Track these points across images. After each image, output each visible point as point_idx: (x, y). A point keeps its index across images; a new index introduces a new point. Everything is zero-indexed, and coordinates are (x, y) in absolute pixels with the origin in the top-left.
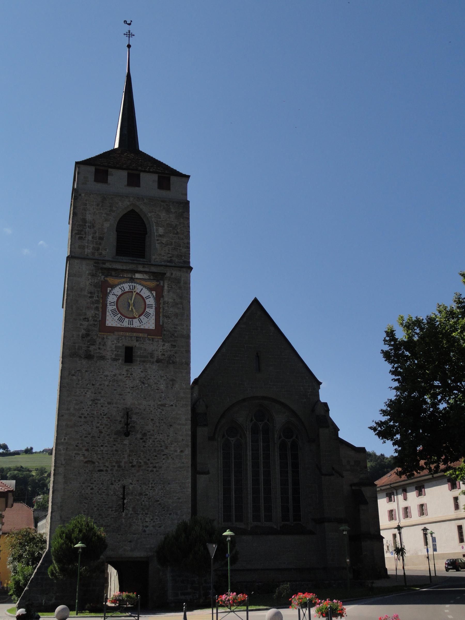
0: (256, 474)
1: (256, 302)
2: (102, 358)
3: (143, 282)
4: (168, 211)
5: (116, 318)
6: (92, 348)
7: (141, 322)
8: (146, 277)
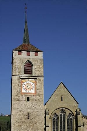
2: (22, 100)
7: (31, 91)
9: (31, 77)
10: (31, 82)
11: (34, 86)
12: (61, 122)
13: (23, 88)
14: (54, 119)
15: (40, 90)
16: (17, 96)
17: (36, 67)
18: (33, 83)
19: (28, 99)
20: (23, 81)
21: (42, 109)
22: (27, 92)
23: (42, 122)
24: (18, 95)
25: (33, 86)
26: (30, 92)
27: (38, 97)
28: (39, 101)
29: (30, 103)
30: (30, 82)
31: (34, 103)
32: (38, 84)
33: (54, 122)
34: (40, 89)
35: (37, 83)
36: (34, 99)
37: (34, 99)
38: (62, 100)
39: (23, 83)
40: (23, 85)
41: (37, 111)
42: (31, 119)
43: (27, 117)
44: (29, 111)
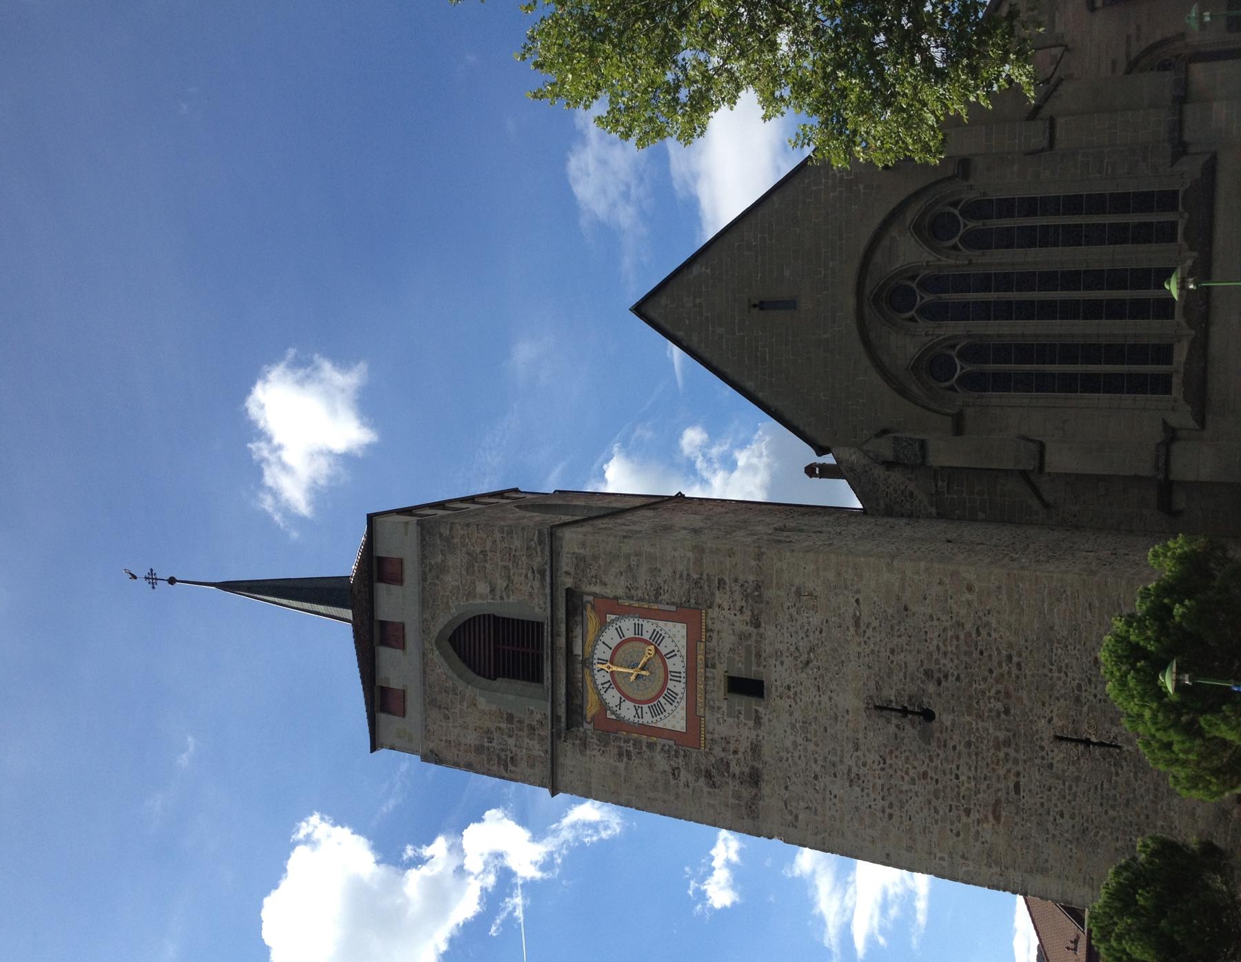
0: (1048, 311)
1: (640, 309)
2: (756, 749)
3: (590, 637)
4: (442, 569)
5: (668, 707)
6: (735, 769)
7: (672, 654)
8: (578, 631)
9: (562, 641)
10: (605, 642)
11: (628, 625)
12: (1008, 311)
13: (647, 719)
14: (974, 383)
15: (666, 572)
16: (717, 779)
17: (482, 588)
18: (603, 626)
19: (746, 687)
20: (591, 709)
21: (831, 575)
22: (679, 688)
23: (970, 589)
24: (708, 775)
25: (629, 634)
26: (677, 665)
27: (719, 598)
28: (755, 595)
29: (776, 675)
30: (602, 652)
31: (774, 637)
32: (615, 587)
33: (1002, 383)
34: (654, 571)
35: (609, 592)
36: (743, 637)
37: (743, 637)
38: (789, 305)
39: (609, 715)
40: (627, 711)
41: (850, 622)
42: (931, 688)
43: (911, 732)
44: (850, 701)
